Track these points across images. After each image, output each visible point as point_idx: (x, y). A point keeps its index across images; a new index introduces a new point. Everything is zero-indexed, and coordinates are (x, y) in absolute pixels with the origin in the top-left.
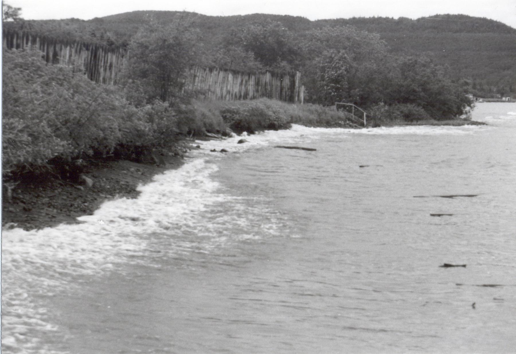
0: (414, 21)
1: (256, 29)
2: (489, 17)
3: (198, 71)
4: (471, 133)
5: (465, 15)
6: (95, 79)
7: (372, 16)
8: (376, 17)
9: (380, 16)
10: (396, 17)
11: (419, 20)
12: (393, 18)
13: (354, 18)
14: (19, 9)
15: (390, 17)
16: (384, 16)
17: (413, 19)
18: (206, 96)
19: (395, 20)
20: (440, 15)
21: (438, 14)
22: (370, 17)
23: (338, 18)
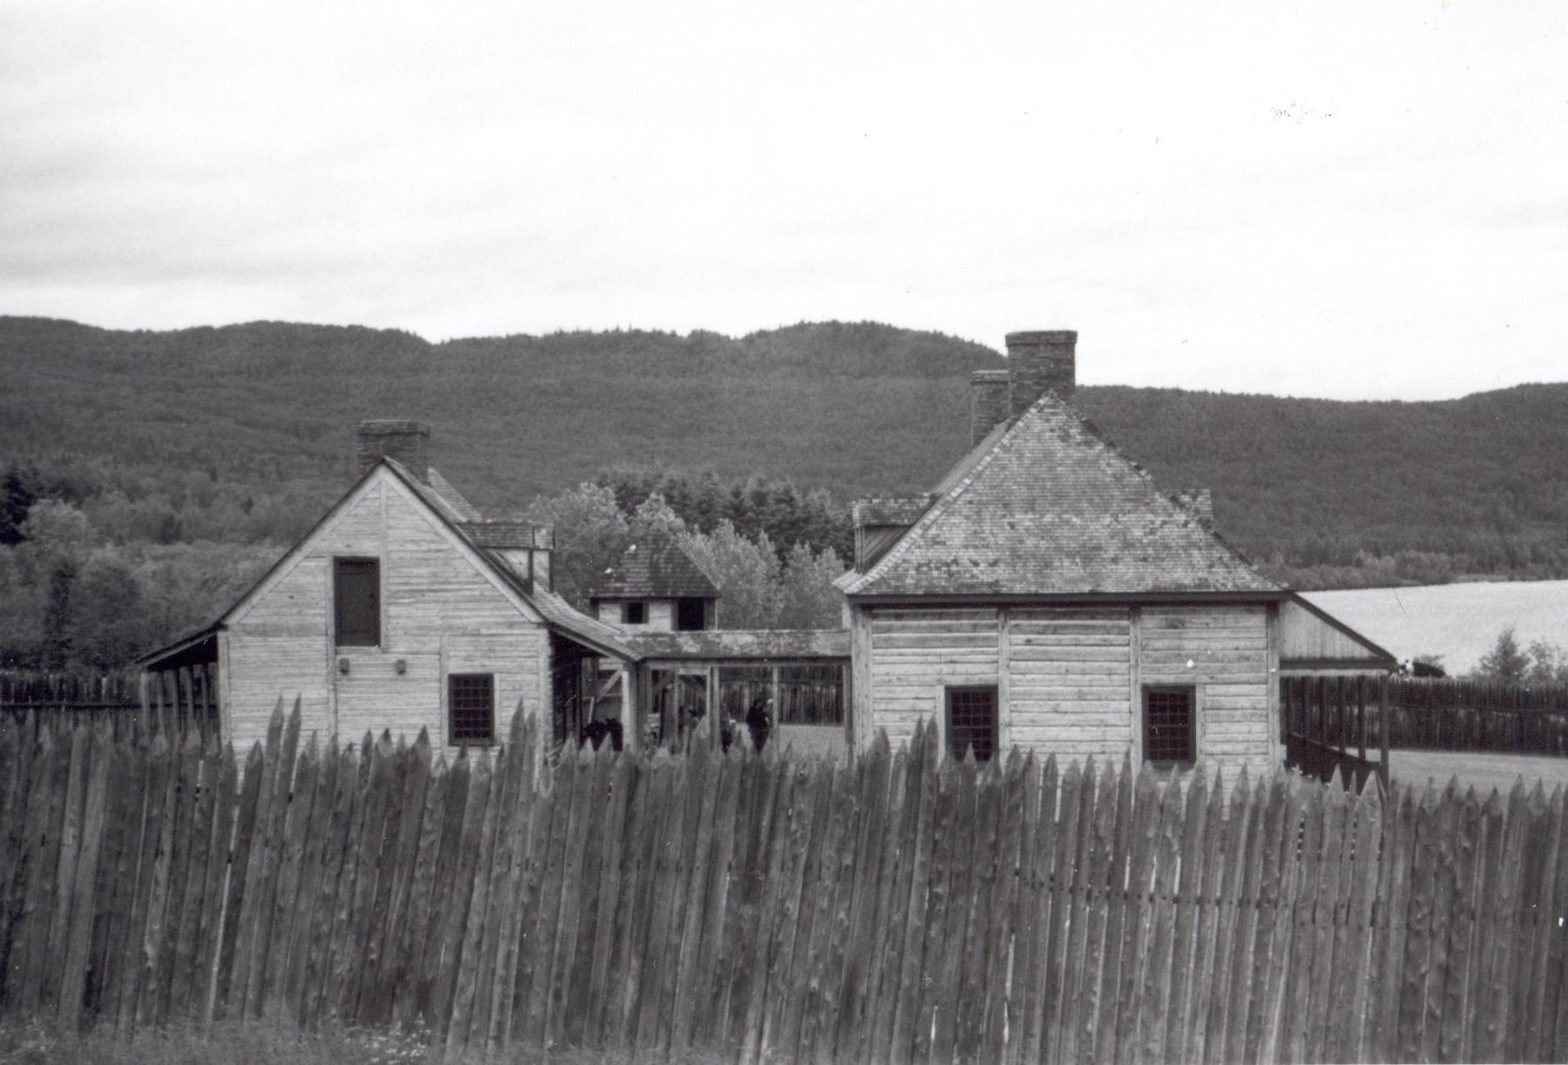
0: (736, 341)
1: (1495, 577)
2: (949, 332)
3: (1127, 767)
4: (477, 593)
5: (883, 325)
6: (685, 747)
7: (611, 327)
8: (625, 329)
9: (635, 326)
10: (684, 332)
11: (750, 340)
12: (673, 335)
13: (560, 335)
14: (1507, 648)
15: (667, 330)
16: (647, 326)
17: (732, 338)
18: (1452, 996)
19: (681, 338)
20: (810, 324)
21: (806, 321)
22: (606, 332)
23: (513, 332)
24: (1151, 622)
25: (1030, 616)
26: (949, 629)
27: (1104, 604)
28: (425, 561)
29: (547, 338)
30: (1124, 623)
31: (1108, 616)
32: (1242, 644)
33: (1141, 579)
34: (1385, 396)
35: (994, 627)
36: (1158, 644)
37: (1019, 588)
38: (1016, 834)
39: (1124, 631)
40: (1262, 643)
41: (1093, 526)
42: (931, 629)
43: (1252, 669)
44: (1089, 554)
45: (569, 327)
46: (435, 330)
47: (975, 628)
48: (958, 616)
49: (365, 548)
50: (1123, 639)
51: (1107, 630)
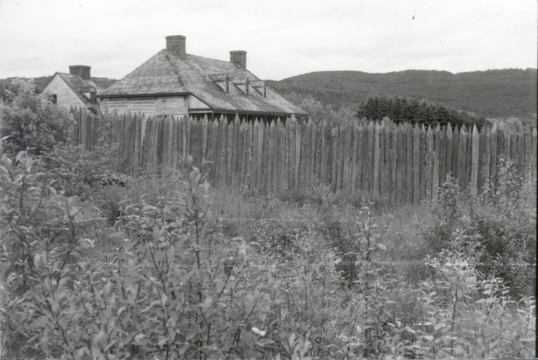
8: (507, 68)
13: (489, 71)
24: (159, 101)
25: (134, 100)
26: (117, 103)
27: (148, 97)
28: (65, 95)
29: (486, 72)
30: (154, 101)
31: (150, 99)
32: (179, 105)
33: (148, 91)
34: (483, 68)
35: (126, 103)
36: (161, 106)
37: (130, 93)
38: (269, 167)
39: (153, 103)
40: (183, 105)
41: (156, 79)
42: (114, 103)
43: (181, 111)
44: (150, 86)
45: (492, 68)
46: (455, 70)
47: (123, 103)
48: (119, 100)
49: (54, 92)
50: (153, 105)
51: (150, 103)
